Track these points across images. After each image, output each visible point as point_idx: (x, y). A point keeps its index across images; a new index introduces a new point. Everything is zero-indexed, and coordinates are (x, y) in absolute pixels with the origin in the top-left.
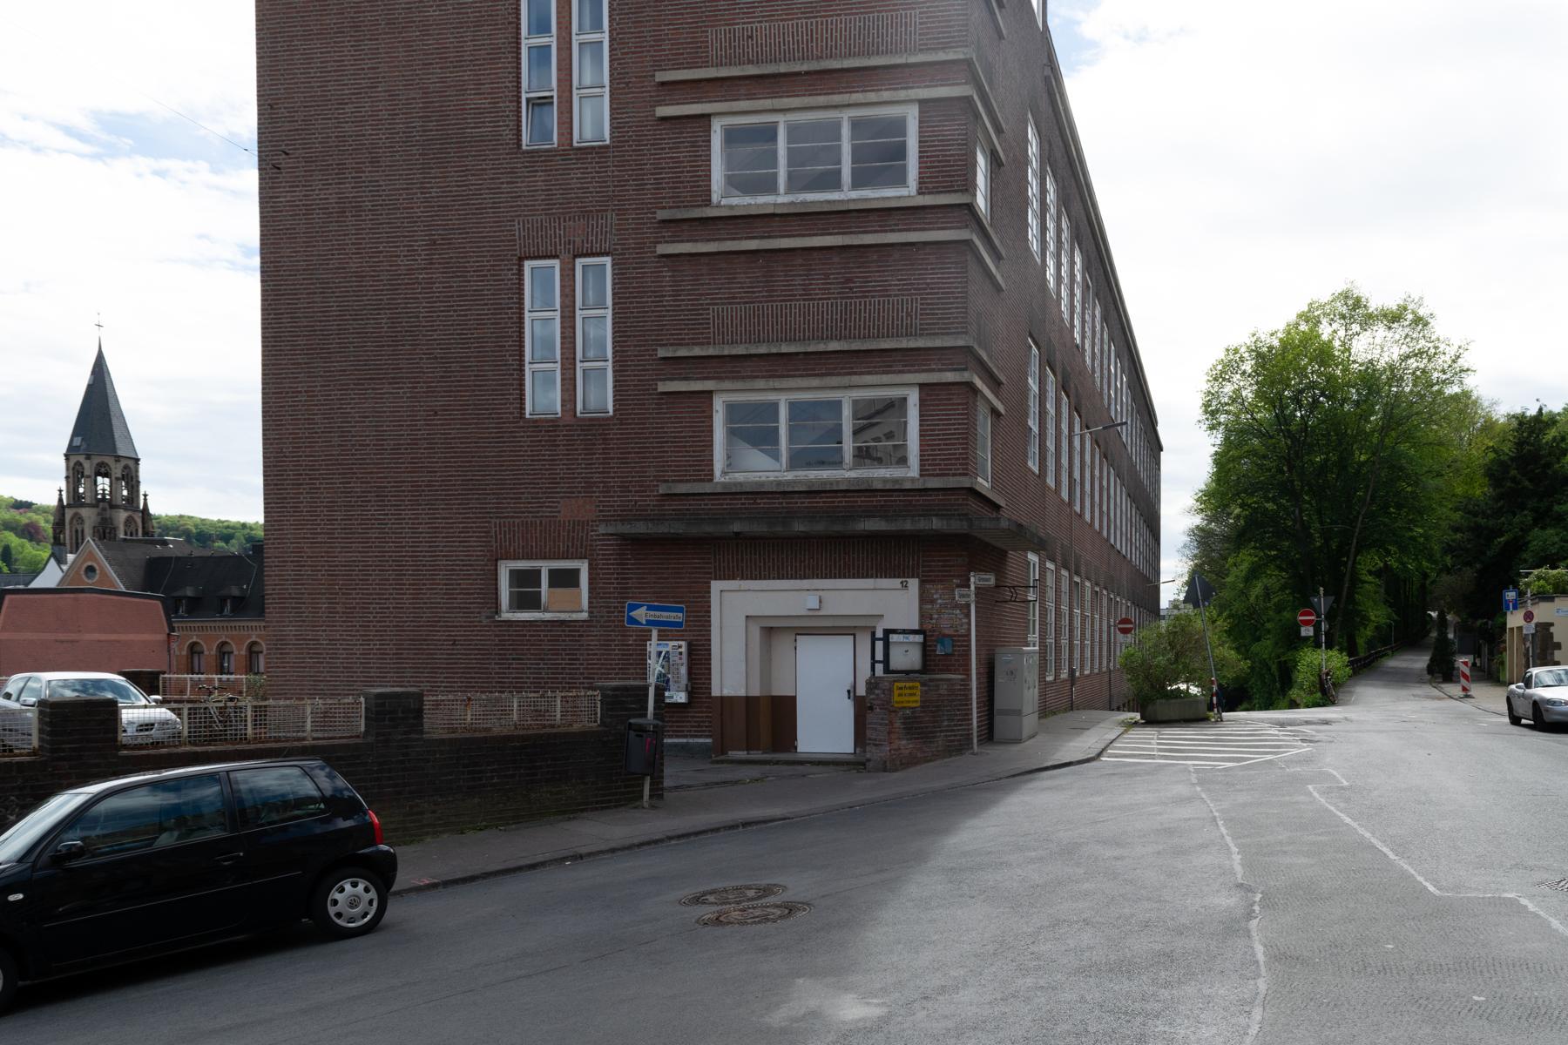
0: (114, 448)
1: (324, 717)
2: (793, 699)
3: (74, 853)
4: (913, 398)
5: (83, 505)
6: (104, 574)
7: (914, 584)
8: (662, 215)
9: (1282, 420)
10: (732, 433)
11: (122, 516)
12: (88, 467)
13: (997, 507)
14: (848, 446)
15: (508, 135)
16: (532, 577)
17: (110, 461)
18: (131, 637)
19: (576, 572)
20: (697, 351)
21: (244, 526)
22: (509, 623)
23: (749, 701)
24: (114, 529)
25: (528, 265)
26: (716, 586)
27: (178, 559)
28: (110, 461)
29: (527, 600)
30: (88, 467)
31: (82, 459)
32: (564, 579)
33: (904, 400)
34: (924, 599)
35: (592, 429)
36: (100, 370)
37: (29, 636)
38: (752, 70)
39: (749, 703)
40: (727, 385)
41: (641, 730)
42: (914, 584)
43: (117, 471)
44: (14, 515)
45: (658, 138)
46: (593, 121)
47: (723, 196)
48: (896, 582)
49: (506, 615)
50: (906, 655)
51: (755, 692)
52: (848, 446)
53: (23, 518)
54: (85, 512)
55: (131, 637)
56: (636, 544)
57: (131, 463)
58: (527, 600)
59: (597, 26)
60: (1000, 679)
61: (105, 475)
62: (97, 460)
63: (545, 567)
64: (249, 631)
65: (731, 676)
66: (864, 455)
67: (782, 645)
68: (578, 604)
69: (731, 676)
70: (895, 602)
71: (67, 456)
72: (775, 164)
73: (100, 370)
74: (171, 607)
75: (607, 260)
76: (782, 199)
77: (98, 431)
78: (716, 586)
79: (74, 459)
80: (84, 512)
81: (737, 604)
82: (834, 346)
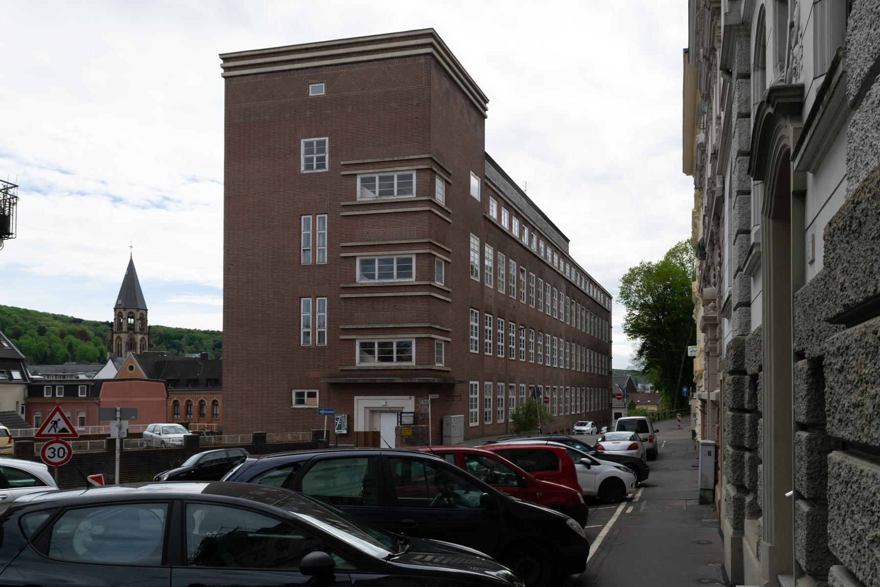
0: (137, 305)
1: (243, 439)
2: (379, 433)
3: (202, 464)
4: (414, 342)
5: (122, 332)
6: (137, 369)
7: (413, 398)
8: (342, 285)
9: (644, 306)
10: (361, 352)
11: (139, 337)
12: (125, 314)
13: (448, 371)
14: (395, 355)
15: (297, 260)
16: (302, 394)
17: (134, 311)
18: (152, 399)
19: (315, 393)
20: (351, 327)
21: (189, 331)
22: (295, 409)
23: (365, 433)
24: (135, 344)
25: (302, 299)
26: (356, 398)
27: (169, 362)
28: (134, 311)
29: (301, 401)
30: (125, 314)
31: (122, 310)
32: (312, 395)
33: (411, 342)
34: (416, 402)
35: (320, 350)
36: (131, 268)
37: (111, 399)
38: (368, 243)
39: (365, 433)
40: (360, 337)
41: (322, 442)
42: (413, 398)
43: (138, 316)
44: (72, 327)
45: (341, 262)
46: (322, 258)
47: (360, 280)
48: (408, 397)
49: (295, 406)
50: (408, 420)
51: (367, 430)
52: (395, 355)
53: (79, 328)
54: (122, 336)
55: (152, 399)
56: (335, 386)
57: (144, 312)
58: (301, 401)
59: (324, 229)
60: (445, 426)
61: (131, 318)
62: (128, 311)
63: (306, 391)
64: (207, 397)
65: (360, 426)
66: (399, 359)
67: (376, 416)
68: (313, 403)
69: (360, 426)
70: (407, 404)
71: (115, 309)
72: (374, 271)
73: (131, 268)
74: (168, 383)
75: (326, 299)
76: (376, 281)
77: (131, 294)
78: (356, 398)
79: (118, 311)
80: (122, 336)
81: (362, 404)
82: (391, 326)
